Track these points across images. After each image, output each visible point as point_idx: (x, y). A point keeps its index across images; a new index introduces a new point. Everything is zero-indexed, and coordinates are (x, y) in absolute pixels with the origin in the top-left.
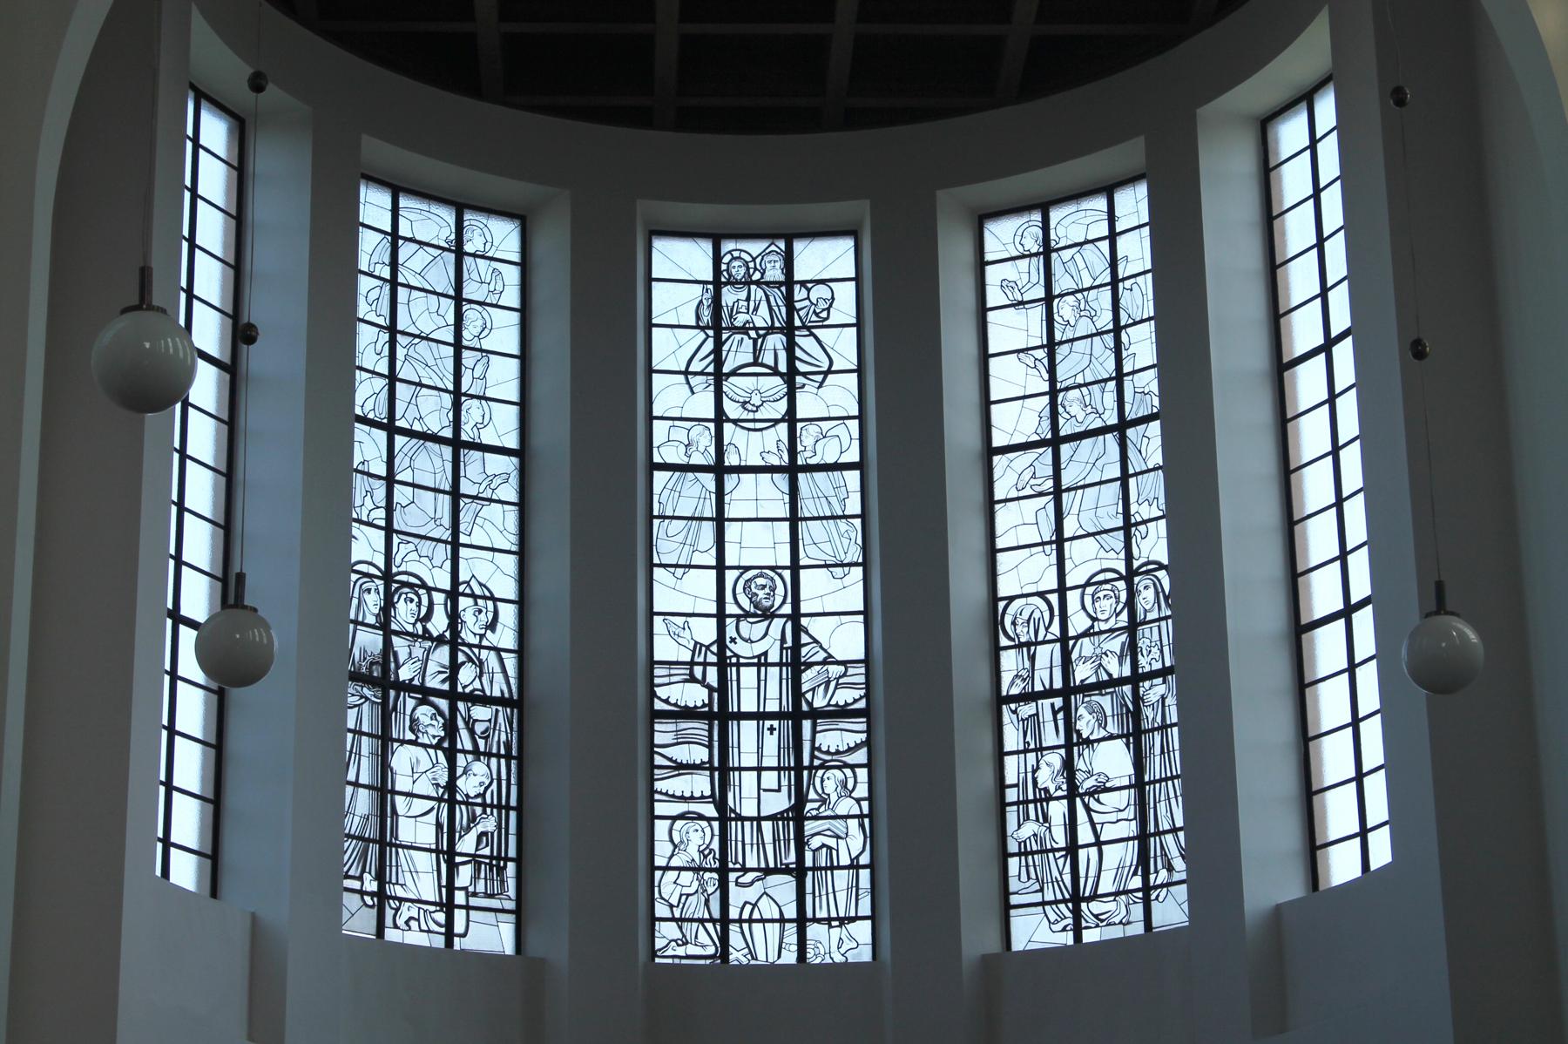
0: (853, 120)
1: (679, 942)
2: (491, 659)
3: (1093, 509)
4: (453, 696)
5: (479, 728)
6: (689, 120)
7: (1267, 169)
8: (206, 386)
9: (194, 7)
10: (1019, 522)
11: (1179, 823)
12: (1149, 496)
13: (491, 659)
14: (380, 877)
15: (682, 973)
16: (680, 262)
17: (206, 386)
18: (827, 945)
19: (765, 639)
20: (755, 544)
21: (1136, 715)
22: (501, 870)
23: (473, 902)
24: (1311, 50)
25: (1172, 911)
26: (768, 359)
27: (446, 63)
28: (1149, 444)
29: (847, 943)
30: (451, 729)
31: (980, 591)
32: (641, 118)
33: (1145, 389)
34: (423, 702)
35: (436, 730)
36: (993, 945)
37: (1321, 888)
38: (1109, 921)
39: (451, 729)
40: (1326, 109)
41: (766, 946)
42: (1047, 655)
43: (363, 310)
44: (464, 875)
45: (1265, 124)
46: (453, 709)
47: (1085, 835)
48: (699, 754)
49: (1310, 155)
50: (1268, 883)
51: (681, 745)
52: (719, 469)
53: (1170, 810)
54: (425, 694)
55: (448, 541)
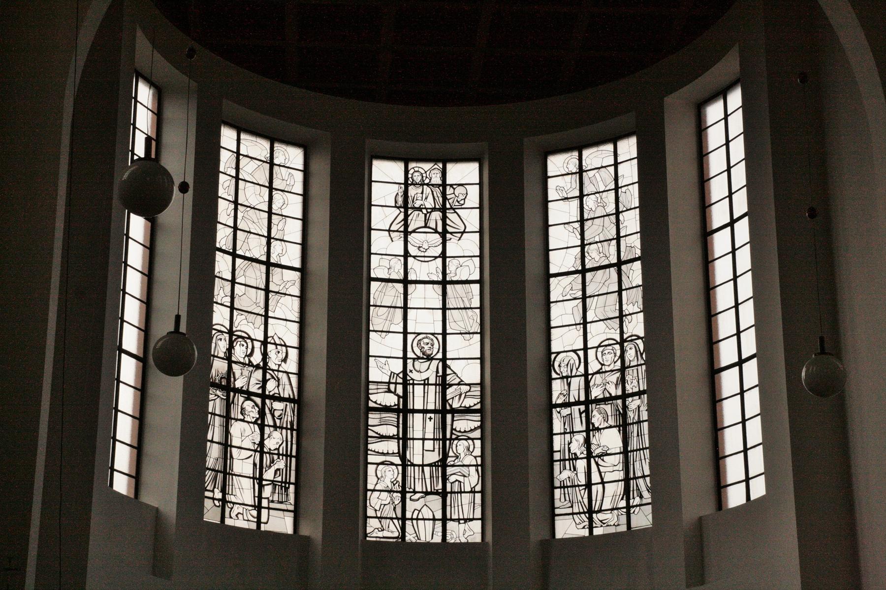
1: (379, 530)
5: (277, 414)
9: (139, 33)
10: (563, 313)
12: (634, 302)
14: (223, 491)
15: (381, 546)
16: (386, 174)
18: (458, 533)
19: (428, 371)
20: (425, 313)
21: (624, 415)
22: (287, 489)
23: (272, 505)
25: (643, 519)
26: (432, 224)
28: (635, 274)
29: (465, 532)
30: (262, 413)
33: (633, 244)
35: (253, 414)
38: (609, 523)
39: (262, 413)
40: (735, 98)
41: (425, 532)
42: (577, 383)
43: (221, 192)
44: (267, 491)
46: (264, 403)
47: (595, 478)
48: (392, 431)
49: (725, 123)
50: (694, 505)
51: (382, 426)
53: (642, 466)
54: (249, 395)
55: (262, 317)
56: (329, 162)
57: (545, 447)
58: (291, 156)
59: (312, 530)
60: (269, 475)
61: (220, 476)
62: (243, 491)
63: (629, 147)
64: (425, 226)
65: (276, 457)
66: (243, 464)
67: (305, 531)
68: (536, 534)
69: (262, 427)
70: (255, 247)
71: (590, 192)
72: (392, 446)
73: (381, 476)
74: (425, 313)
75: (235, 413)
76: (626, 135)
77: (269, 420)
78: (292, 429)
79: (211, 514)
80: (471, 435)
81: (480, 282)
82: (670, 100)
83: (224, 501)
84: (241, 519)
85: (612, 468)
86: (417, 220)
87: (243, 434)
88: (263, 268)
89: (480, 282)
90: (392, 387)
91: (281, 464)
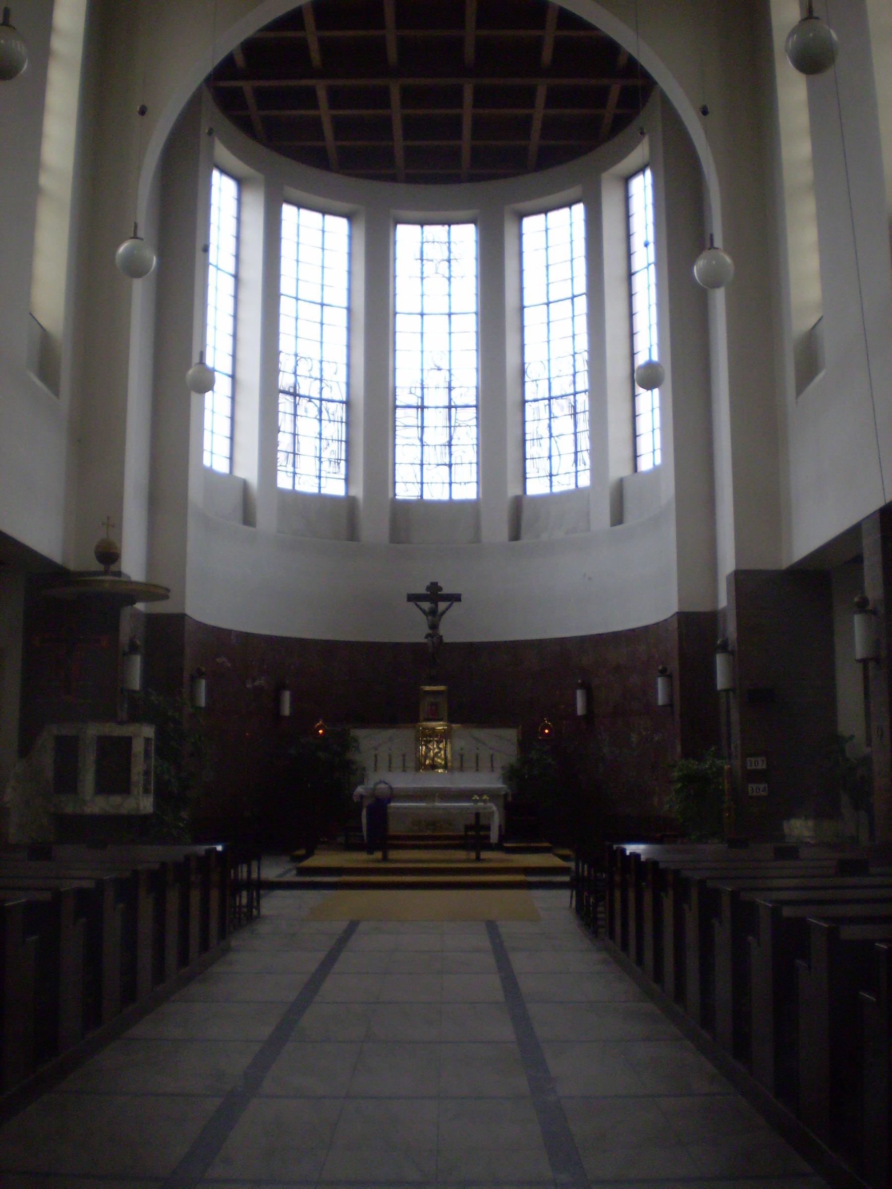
0: (474, 178)
1: (405, 491)
2: (334, 385)
3: (561, 329)
4: (321, 400)
5: (330, 411)
6: (411, 179)
7: (627, 198)
8: (222, 384)
11: (587, 408)
13: (334, 385)
14: (294, 465)
15: (406, 503)
17: (222, 384)
19: (441, 378)
20: (436, 346)
21: (574, 407)
22: (339, 464)
23: (328, 475)
24: (641, 152)
25: (585, 480)
26: (440, 271)
27: (317, 159)
31: (518, 361)
32: (393, 179)
34: (310, 401)
35: (315, 412)
36: (518, 492)
37: (639, 470)
40: (648, 173)
41: (436, 493)
44: (325, 465)
45: (627, 180)
46: (321, 404)
47: (546, 363)
49: (642, 188)
50: (618, 469)
52: (422, 407)
53: (585, 443)
54: (310, 399)
55: (318, 344)
56: (363, 229)
57: (520, 432)
58: (338, 226)
59: (358, 491)
60: (326, 455)
61: (291, 456)
62: (307, 465)
63: (579, 209)
64: (436, 257)
65: (330, 442)
66: (307, 446)
67: (353, 493)
68: (513, 491)
69: (320, 420)
70: (310, 291)
71: (552, 240)
72: (416, 432)
73: (405, 452)
74: (436, 346)
75: (300, 411)
76: (577, 202)
77: (325, 416)
78: (342, 422)
79: (284, 482)
80: (469, 423)
81: (476, 406)
82: (605, 176)
83: (295, 474)
84: (307, 485)
85: (565, 445)
86: (429, 267)
87: (307, 426)
88: (319, 306)
89: (476, 406)
90: (413, 390)
91: (334, 446)
